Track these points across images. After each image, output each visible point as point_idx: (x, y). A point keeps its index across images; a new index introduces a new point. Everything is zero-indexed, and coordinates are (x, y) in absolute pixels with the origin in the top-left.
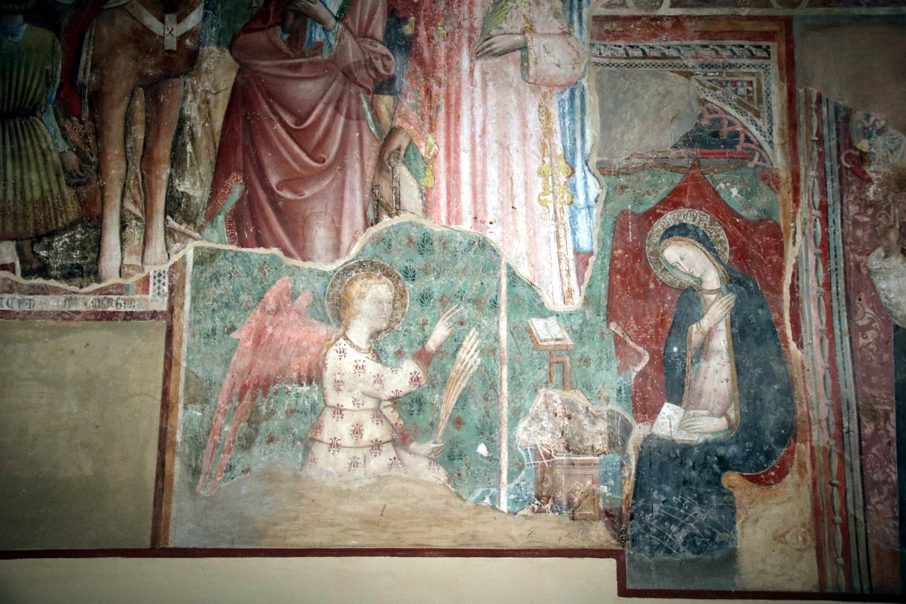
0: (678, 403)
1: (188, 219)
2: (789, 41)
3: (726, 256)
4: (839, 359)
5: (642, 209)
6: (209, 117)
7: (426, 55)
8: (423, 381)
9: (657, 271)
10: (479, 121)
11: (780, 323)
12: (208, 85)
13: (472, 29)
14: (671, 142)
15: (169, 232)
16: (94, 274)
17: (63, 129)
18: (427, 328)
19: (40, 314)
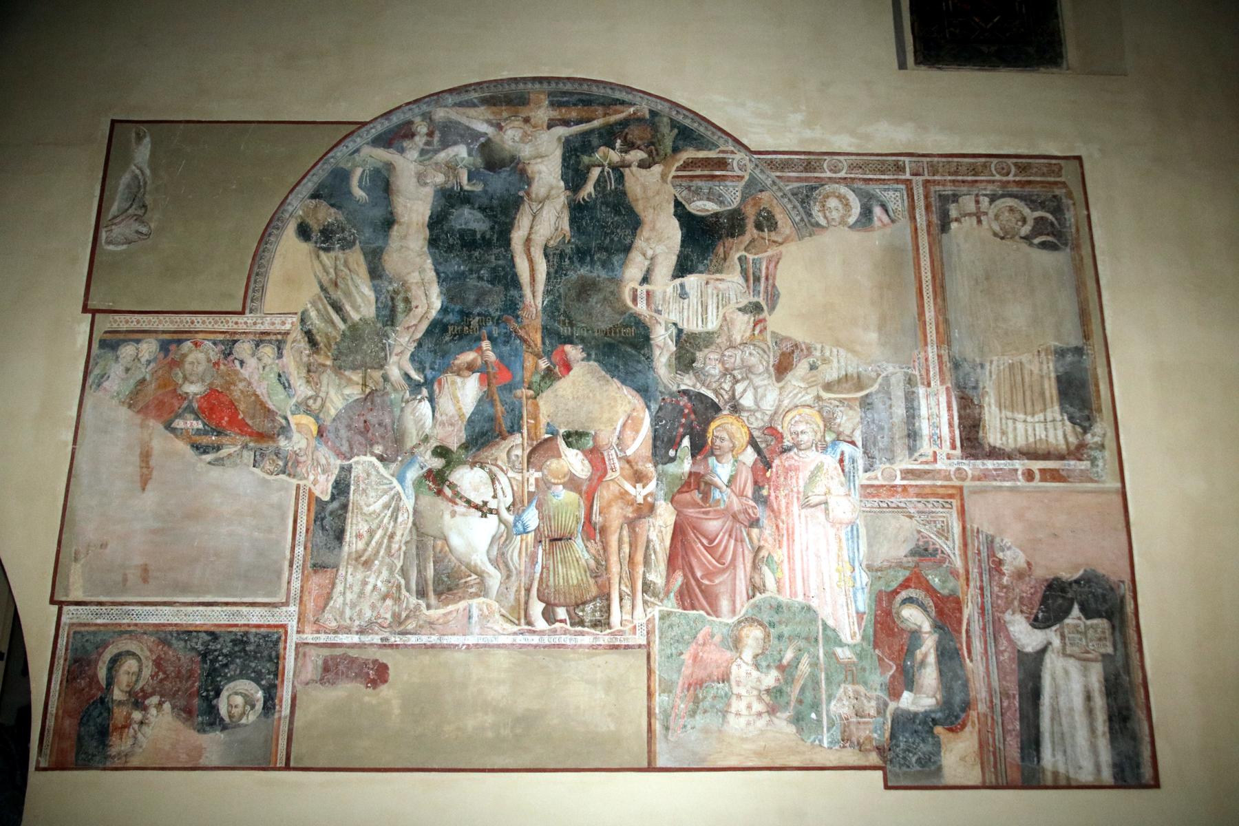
0: (911, 691)
1: (655, 595)
2: (962, 499)
3: (933, 614)
5: (890, 589)
6: (662, 540)
7: (775, 506)
9: (898, 622)
11: (961, 649)
12: (661, 523)
13: (798, 492)
15: (645, 602)
16: (608, 625)
19: (581, 646)
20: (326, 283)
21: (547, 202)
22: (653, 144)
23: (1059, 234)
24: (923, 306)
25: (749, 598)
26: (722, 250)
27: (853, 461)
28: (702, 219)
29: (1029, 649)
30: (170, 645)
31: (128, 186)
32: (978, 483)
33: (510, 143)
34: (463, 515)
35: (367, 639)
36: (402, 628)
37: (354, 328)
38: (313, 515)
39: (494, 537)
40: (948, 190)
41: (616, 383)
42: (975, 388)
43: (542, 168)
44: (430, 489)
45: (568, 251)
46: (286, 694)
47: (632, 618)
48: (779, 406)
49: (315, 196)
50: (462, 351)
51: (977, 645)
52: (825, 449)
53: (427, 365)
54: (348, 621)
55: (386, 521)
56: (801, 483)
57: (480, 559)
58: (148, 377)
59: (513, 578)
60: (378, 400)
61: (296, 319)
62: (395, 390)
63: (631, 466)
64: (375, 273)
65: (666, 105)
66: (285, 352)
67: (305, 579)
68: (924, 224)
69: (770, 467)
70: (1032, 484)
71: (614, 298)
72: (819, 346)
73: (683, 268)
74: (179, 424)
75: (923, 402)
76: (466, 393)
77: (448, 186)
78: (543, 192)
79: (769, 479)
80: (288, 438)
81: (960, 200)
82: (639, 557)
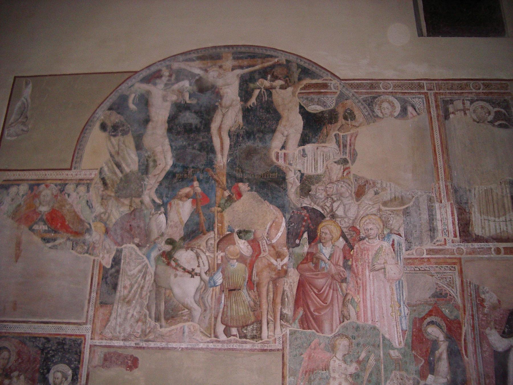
0: (433, 374)
1: (287, 321)
2: (461, 265)
3: (445, 330)
4: (478, 360)
5: (421, 317)
6: (292, 290)
7: (356, 271)
8: (359, 369)
9: (425, 335)
10: (372, 291)
11: (461, 350)
12: (291, 280)
13: (369, 262)
14: (428, 296)
15: (281, 325)
16: (260, 338)
17: (249, 294)
18: (359, 354)
19: (245, 349)
20: (113, 153)
21: (231, 108)
22: (287, 76)
23: (508, 120)
24: (436, 159)
25: (340, 323)
26: (325, 131)
27: (400, 244)
28: (315, 114)
29: (500, 350)
30: (25, 344)
31: (20, 108)
32: (469, 256)
33: (212, 79)
34: (181, 276)
35: (127, 344)
36: (146, 338)
37: (126, 176)
38: (101, 275)
39: (197, 288)
40: (448, 98)
41: (267, 203)
42: (466, 203)
43: (228, 90)
44: (164, 262)
45: (242, 133)
46: (84, 372)
47: (273, 334)
48: (358, 214)
49: (110, 109)
50: (183, 187)
51: (471, 348)
52: (383, 239)
53: (164, 195)
54: (118, 333)
55: (139, 279)
56: (370, 257)
57: (190, 301)
58: (22, 203)
59: (208, 312)
60: (138, 214)
61: (97, 172)
62: (147, 209)
63: (275, 249)
64: (139, 147)
65: (295, 57)
66: (91, 189)
67: (96, 310)
68: (436, 115)
69: (353, 249)
70: (500, 256)
71: (266, 157)
72: (380, 182)
73: (304, 141)
74: (36, 227)
75: (438, 212)
76: (184, 210)
77: (179, 101)
78: (228, 103)
79: (352, 256)
80: (90, 234)
81: (455, 103)
82: (279, 300)
